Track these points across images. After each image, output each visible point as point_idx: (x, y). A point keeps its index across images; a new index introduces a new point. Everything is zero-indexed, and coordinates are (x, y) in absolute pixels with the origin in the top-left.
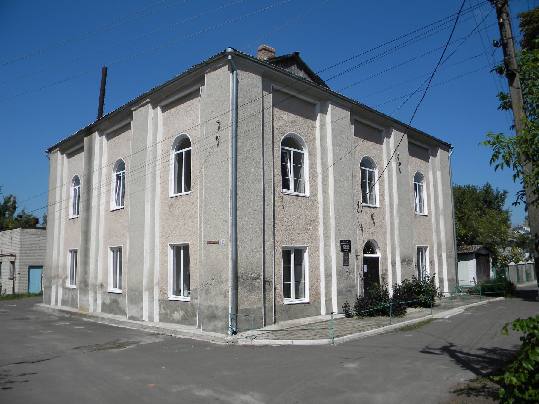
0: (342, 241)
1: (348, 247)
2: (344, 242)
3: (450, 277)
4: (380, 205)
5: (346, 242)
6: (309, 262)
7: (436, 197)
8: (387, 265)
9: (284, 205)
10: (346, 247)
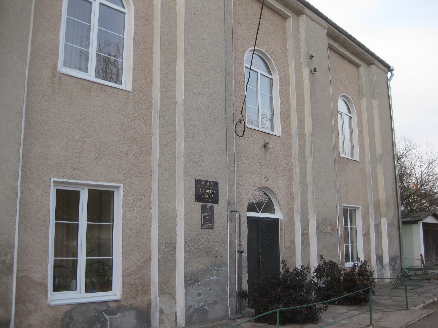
0: (198, 182)
1: (212, 194)
2: (203, 183)
3: (393, 254)
4: (282, 133)
5: (208, 184)
6: (124, 217)
7: (361, 132)
8: (293, 232)
9: (226, 153)
10: (207, 193)
